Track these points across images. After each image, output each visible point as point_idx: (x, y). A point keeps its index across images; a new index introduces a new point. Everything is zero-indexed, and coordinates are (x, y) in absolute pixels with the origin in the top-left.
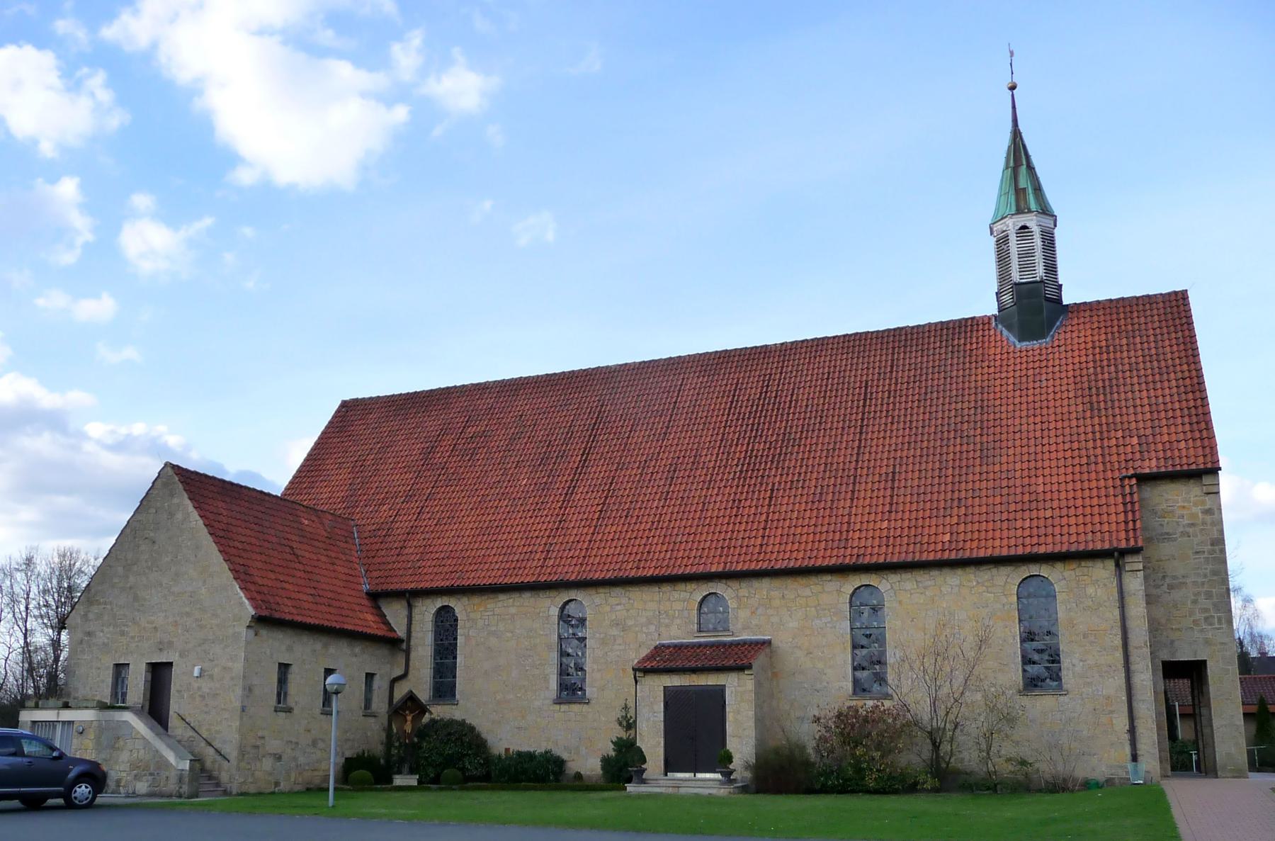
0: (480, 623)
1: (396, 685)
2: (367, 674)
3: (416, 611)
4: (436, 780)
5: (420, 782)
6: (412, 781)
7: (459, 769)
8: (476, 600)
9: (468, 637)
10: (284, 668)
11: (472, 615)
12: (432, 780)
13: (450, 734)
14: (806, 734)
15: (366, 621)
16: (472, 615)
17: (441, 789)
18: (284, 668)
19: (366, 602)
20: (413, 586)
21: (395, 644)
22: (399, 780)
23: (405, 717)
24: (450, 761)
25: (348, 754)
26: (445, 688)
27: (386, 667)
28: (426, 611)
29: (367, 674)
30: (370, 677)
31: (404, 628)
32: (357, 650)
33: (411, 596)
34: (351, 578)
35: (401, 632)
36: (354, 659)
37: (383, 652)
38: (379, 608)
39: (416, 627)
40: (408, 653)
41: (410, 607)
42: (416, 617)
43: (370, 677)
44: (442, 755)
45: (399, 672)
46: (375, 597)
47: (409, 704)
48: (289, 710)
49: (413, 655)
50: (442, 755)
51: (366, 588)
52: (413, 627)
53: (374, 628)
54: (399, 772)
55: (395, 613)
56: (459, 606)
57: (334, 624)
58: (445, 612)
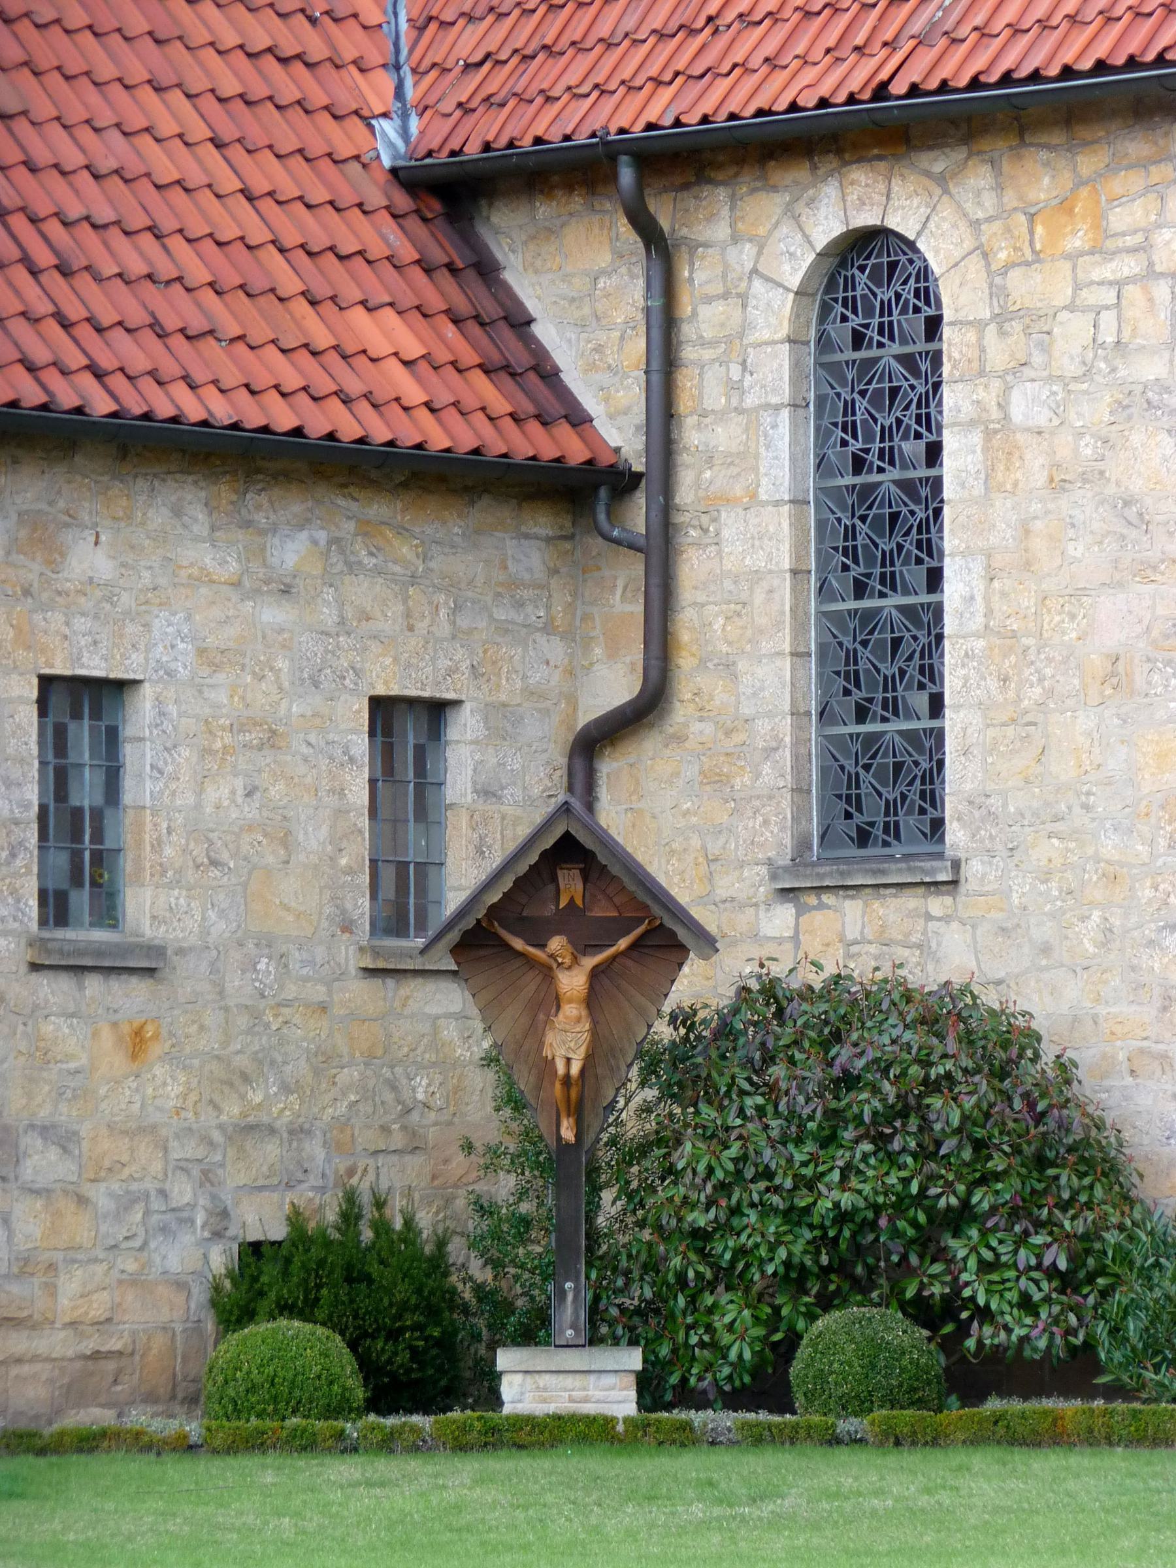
0: (1073, 333)
1: (609, 767)
2: (384, 711)
3: (698, 277)
4: (765, 1387)
5: (649, 1387)
6: (604, 1384)
7: (922, 1312)
8: (1041, 175)
9: (997, 432)
10: (81, 705)
11: (1024, 287)
12: (722, 1378)
13: (849, 1081)
14: (948, 893)
15: (391, 367)
16: (1024, 287)
17: (790, 1438)
18: (81, 705)
19: (387, 237)
20: (660, 108)
21: (587, 498)
22: (528, 1384)
23: (547, 973)
24: (844, 1265)
25: (264, 1221)
26: (880, 793)
27: (515, 655)
28: (757, 264)
29: (384, 711)
30: (406, 726)
31: (632, 394)
32: (293, 551)
33: (668, 170)
34: (288, 84)
35: (620, 432)
36: (273, 614)
37: (521, 547)
38: (486, 270)
39: (702, 385)
40: (660, 556)
41: (660, 248)
42: (703, 319)
43: (406, 726)
44: (795, 1216)
45: (614, 686)
46: (453, 193)
47: (571, 885)
48: (145, 964)
49: (694, 569)
50: (795, 1216)
51: (389, 142)
52: (686, 381)
53: (473, 419)
54: (533, 1331)
55: (574, 288)
56: (942, 216)
57: (317, 423)
58: (873, 300)
